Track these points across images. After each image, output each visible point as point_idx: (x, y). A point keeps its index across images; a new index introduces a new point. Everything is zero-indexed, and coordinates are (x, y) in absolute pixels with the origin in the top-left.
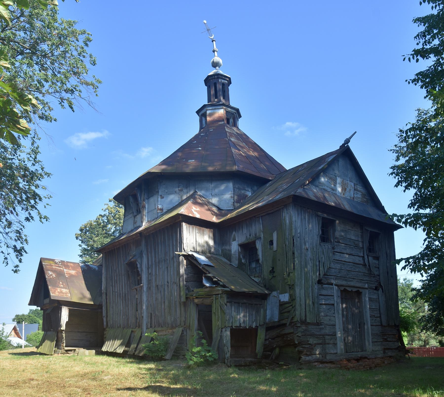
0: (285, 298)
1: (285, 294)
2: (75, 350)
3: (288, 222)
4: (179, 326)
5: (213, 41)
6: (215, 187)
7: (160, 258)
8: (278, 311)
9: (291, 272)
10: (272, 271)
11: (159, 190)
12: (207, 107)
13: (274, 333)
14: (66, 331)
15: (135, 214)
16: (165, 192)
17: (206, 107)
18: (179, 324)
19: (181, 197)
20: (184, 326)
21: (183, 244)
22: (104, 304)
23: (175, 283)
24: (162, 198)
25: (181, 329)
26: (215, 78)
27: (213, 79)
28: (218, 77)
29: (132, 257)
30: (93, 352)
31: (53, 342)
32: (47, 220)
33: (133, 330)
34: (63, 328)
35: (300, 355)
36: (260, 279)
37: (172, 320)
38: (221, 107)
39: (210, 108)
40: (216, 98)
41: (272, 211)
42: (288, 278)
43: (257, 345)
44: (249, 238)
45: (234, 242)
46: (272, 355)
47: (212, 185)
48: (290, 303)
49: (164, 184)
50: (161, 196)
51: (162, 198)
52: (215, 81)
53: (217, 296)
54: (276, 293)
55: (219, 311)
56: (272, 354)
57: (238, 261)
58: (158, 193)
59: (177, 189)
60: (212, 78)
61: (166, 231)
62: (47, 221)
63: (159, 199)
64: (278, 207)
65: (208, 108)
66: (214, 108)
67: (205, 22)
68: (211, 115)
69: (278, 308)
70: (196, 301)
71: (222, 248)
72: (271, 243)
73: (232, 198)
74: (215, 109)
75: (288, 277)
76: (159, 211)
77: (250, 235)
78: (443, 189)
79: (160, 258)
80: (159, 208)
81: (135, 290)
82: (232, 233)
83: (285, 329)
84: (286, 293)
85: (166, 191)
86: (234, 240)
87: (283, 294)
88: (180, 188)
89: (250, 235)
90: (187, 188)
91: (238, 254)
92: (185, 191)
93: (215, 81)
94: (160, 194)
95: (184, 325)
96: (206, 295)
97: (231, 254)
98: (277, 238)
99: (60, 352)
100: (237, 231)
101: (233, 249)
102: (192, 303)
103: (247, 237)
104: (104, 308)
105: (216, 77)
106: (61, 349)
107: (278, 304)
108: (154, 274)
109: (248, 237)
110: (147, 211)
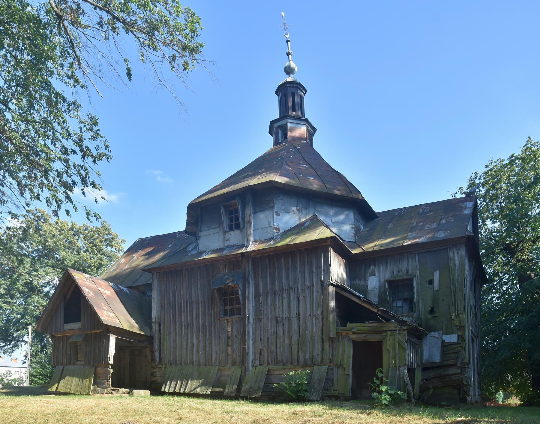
0: (452, 338)
1: (452, 335)
2: (118, 390)
3: (457, 262)
4: (318, 363)
5: (287, 41)
6: (336, 215)
7: (284, 286)
8: (440, 351)
9: (461, 313)
10: (432, 311)
11: (275, 206)
12: (288, 119)
13: (432, 374)
14: (113, 366)
15: (226, 229)
16: (282, 209)
17: (286, 119)
18: (319, 361)
19: (300, 219)
20: (330, 364)
21: (331, 272)
22: (156, 335)
23: (314, 316)
24: (278, 215)
25: (325, 368)
26: (293, 87)
27: (291, 88)
28: (297, 86)
29: (230, 281)
30: (148, 393)
31: (88, 380)
32: (97, 219)
33: (220, 368)
34: (111, 362)
35: (465, 395)
36: (411, 319)
37: (307, 357)
38: (304, 123)
39: (292, 121)
40: (293, 111)
41: (436, 249)
42: (456, 319)
43: (415, 385)
44: (397, 275)
45: (373, 277)
46: (423, 396)
47: (332, 212)
48: (460, 344)
49: (281, 199)
50: (276, 212)
51: (278, 215)
52: (293, 90)
53: (391, 332)
54: (436, 334)
55: (397, 348)
56: (424, 395)
57: (379, 298)
58: (274, 208)
59: (294, 208)
60: (290, 85)
61: (298, 255)
62: (97, 220)
63: (275, 216)
64: (444, 246)
65: (289, 121)
66: (296, 122)
67: (283, 14)
68: (292, 130)
69: (440, 348)
70: (353, 337)
71: (352, 283)
72: (431, 282)
73: (353, 229)
74: (297, 123)
75: (456, 318)
76: (275, 231)
77: (399, 272)
78: (539, 253)
79: (284, 286)
80: (275, 227)
81: (226, 321)
82: (370, 267)
83: (448, 370)
84: (453, 334)
85: (283, 207)
86: (373, 274)
87: (448, 335)
88: (298, 208)
89: (399, 272)
90: (306, 209)
91: (378, 290)
92: (304, 211)
93: (293, 90)
94: (275, 210)
95: (330, 363)
96: (373, 331)
97: (367, 290)
98: (440, 278)
99: (105, 392)
100: (377, 266)
101: (371, 285)
102: (346, 339)
103: (393, 273)
104: (156, 342)
105: (295, 86)
106: (106, 388)
107: (440, 345)
108: (269, 304)
109: (395, 273)
110: (254, 228)
